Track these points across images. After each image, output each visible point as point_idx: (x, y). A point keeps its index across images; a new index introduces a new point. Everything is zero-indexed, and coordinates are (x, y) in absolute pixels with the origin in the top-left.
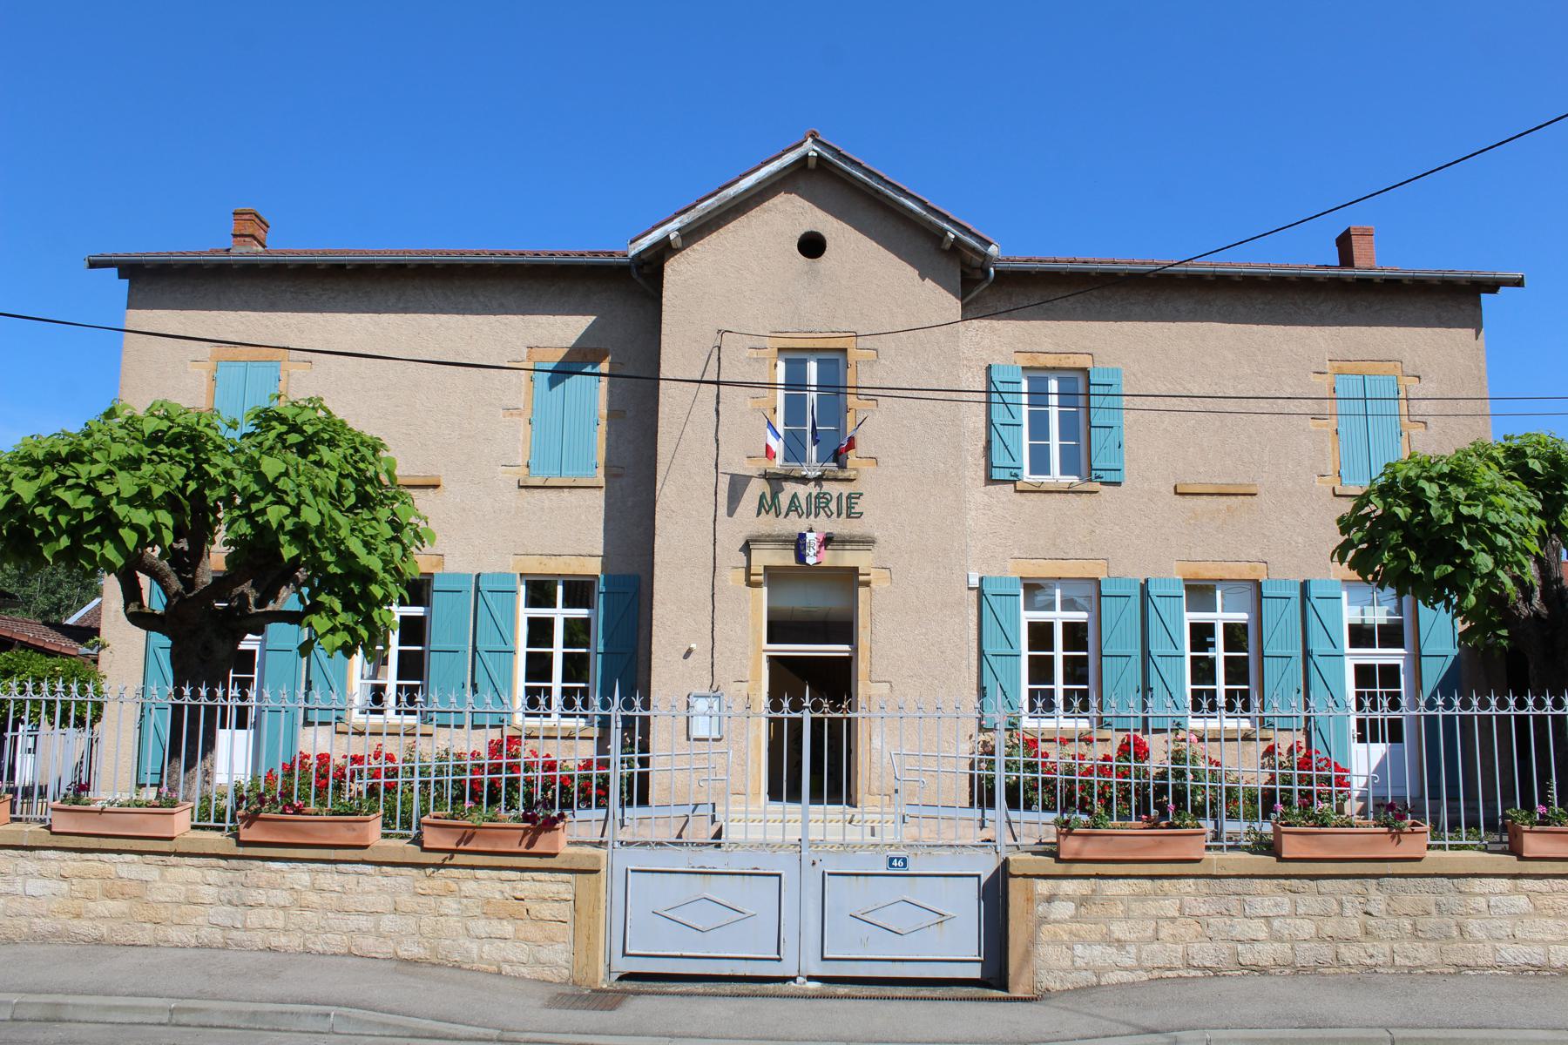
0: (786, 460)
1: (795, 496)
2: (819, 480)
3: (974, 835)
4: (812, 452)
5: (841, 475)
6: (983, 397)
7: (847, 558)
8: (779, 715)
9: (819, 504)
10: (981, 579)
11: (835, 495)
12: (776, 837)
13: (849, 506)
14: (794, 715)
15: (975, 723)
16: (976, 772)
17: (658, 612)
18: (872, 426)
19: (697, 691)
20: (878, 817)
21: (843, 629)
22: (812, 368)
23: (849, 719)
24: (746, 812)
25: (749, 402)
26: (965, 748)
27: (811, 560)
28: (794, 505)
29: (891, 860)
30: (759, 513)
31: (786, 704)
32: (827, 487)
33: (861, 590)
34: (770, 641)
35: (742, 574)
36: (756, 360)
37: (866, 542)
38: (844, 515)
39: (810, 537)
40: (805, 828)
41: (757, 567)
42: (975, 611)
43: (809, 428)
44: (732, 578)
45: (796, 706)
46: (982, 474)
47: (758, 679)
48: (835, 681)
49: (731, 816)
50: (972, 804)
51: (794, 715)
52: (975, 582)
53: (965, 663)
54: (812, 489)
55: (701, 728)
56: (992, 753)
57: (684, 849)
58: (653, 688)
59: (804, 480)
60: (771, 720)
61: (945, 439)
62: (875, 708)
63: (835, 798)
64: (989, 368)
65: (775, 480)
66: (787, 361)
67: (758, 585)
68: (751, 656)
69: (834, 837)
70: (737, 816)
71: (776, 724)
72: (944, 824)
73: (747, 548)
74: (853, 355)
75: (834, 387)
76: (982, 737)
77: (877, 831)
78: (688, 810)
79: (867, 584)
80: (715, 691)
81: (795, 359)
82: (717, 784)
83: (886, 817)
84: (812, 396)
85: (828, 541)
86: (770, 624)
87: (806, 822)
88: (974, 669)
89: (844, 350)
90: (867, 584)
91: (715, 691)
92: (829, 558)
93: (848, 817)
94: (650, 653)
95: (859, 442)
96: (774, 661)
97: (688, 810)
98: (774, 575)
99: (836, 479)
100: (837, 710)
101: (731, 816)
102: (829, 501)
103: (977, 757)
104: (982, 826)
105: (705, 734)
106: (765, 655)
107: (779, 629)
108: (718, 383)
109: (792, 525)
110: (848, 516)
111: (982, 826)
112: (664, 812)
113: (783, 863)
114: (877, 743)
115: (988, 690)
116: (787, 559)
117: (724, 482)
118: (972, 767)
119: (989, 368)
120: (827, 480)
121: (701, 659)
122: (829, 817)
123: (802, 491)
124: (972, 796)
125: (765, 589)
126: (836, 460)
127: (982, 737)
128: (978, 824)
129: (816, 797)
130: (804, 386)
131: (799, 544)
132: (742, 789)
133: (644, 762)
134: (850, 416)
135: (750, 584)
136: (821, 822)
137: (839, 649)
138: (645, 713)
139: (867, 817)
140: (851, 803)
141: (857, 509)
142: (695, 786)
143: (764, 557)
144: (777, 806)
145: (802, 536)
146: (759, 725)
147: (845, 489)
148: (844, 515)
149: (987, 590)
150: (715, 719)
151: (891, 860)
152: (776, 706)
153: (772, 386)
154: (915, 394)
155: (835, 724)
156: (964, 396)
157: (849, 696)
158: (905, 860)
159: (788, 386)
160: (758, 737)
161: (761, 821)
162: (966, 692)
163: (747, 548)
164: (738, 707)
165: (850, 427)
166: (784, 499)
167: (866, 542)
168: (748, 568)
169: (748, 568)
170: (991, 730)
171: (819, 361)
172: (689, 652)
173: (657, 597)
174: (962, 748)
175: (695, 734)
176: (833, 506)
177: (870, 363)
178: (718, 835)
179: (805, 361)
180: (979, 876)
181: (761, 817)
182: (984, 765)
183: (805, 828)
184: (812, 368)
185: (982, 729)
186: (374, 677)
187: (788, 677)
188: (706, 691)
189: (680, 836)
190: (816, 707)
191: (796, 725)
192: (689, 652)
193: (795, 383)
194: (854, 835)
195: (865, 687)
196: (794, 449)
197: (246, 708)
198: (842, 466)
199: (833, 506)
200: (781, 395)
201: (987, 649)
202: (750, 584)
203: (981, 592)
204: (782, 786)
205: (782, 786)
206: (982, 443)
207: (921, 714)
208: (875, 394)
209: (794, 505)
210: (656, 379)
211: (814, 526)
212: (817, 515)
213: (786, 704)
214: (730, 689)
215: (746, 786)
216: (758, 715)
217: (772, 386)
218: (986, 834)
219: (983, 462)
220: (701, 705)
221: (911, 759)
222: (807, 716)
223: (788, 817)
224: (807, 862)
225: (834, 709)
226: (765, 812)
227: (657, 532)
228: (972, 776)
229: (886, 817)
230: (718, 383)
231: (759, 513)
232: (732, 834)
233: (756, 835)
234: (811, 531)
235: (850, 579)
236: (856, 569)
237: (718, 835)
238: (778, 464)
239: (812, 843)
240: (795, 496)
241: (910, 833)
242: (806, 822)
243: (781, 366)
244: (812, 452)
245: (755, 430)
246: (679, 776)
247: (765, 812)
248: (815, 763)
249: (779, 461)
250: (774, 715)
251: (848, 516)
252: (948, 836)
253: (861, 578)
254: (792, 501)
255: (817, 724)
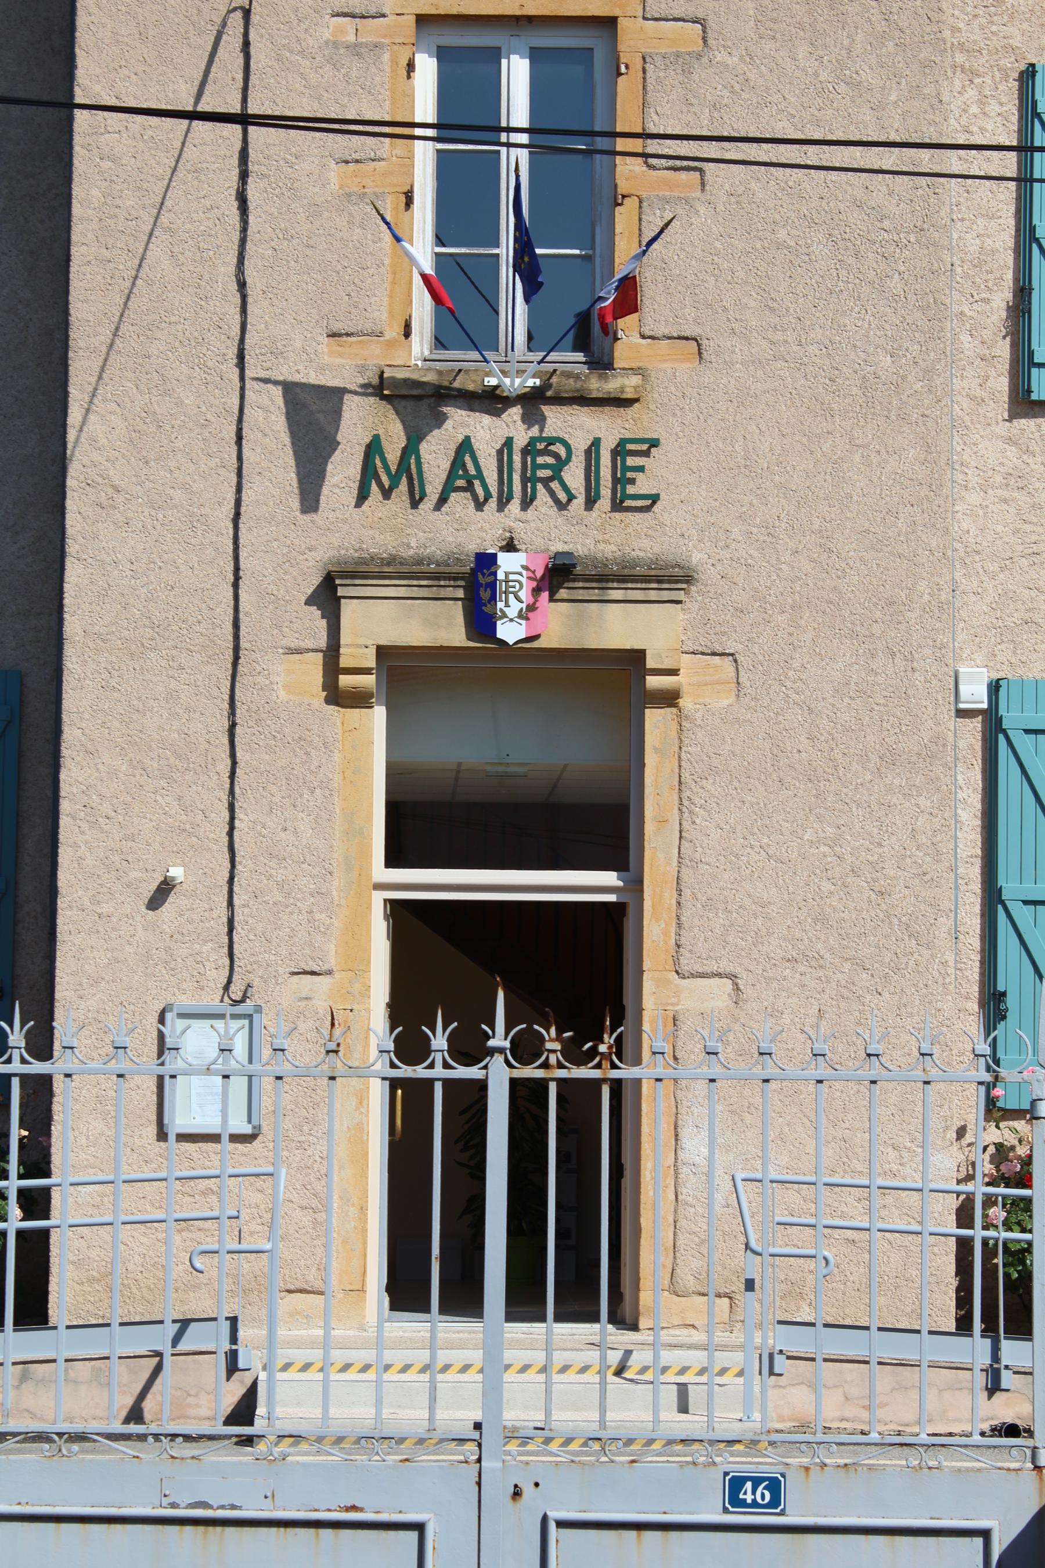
0: (439, 342)
1: (465, 447)
2: (533, 402)
3: (968, 1410)
4: (515, 314)
5: (596, 386)
6: (1008, 163)
7: (615, 625)
8: (420, 1072)
9: (535, 470)
10: (994, 688)
11: (580, 444)
12: (408, 1414)
13: (620, 481)
14: (463, 1072)
15: (976, 1098)
16: (978, 1234)
17: (75, 776)
18: (690, 247)
19: (185, 1001)
20: (697, 1358)
21: (602, 825)
22: (517, 74)
23: (617, 1086)
24: (326, 1344)
25: (334, 174)
26: (945, 1164)
27: (509, 632)
28: (462, 472)
29: (736, 1484)
30: (362, 497)
31: (439, 1042)
32: (558, 420)
33: (655, 719)
34: (394, 859)
35: (314, 668)
36: (355, 49)
37: (668, 579)
38: (604, 503)
39: (508, 563)
40: (492, 1394)
41: (359, 647)
42: (976, 776)
43: (506, 249)
44: (287, 680)
45: (469, 1048)
46: (1003, 384)
47: (359, 967)
48: (578, 975)
49: (283, 1355)
50: (964, 1325)
51: (463, 1072)
52: (975, 693)
53: (945, 923)
54: (512, 425)
55: (196, 1106)
56: (1024, 1180)
57: (148, 1452)
58: (61, 992)
59: (491, 401)
60: (394, 1084)
61: (895, 284)
62: (692, 1050)
63: (578, 1304)
64: (1028, 75)
65: (419, 401)
66: (443, 55)
67: (359, 700)
68: (337, 901)
69: (575, 1415)
70: (300, 1356)
71: (410, 1100)
72: (885, 1378)
73: (327, 596)
74: (633, 37)
75: (578, 138)
76: (993, 1135)
77: (695, 1395)
78: (160, 1338)
79: (669, 699)
80: (237, 1001)
81: (466, 52)
82: (247, 1265)
83: (723, 1359)
84: (516, 161)
85: (558, 575)
86: (394, 810)
87: (493, 1370)
88: (973, 941)
89: (609, 24)
90: (669, 699)
91: (237, 1001)
92: (560, 625)
93: (614, 1358)
94: (53, 892)
95: (649, 293)
96: (406, 917)
97: (160, 1338)
98: (403, 671)
99: (583, 400)
100: (581, 1059)
101: (283, 1355)
102: (561, 463)
103: (979, 1189)
104: (994, 1387)
105: (206, 1121)
106: (378, 898)
107: (414, 830)
108: (243, 120)
109: (460, 529)
110: (617, 506)
111: (994, 1387)
112: (93, 1344)
113: (432, 1494)
114: (695, 1146)
115: (1011, 1002)
116: (443, 626)
117: (269, 415)
118: (964, 1216)
119: (1028, 75)
120: (559, 400)
121: (197, 908)
122: (560, 1358)
123: (486, 432)
124: (964, 1300)
125: (379, 714)
126: (582, 343)
127: (993, 1135)
128: (981, 1380)
129: (523, 1302)
130: (492, 129)
131: (476, 585)
132: (318, 1285)
133: (36, 1203)
134: (624, 217)
135: (336, 696)
136: (537, 1371)
137: (592, 884)
138: (38, 1067)
139: (667, 1357)
140: (624, 1318)
141: (643, 485)
142: (179, 1270)
143: (375, 622)
144: (411, 1327)
145: (486, 562)
146: (362, 1099)
147: (606, 427)
148: (604, 503)
149: (1011, 717)
150: (239, 1084)
151: (736, 1484)
152: (410, 1047)
153: (402, 129)
154: (813, 155)
155: (579, 1098)
156: (954, 162)
157: (618, 1020)
158: (774, 1486)
159: (446, 128)
160: (359, 1131)
161: (366, 1372)
162: (947, 1006)
163: (327, 596)
164: (305, 1051)
165: (625, 249)
166: (436, 455)
167: (668, 579)
168: (332, 651)
169: (332, 651)
170: (1017, 1114)
171: (536, 56)
172: (165, 889)
173: (70, 734)
174: (936, 1161)
175: (180, 1121)
176: (574, 476)
177: (683, 62)
178: (244, 1412)
179: (494, 56)
180: (985, 1534)
181: (368, 1355)
182: (998, 1213)
183: (492, 1394)
184: (517, 74)
185: (995, 1111)
186: (996, 1227)
187: (445, 963)
188: (211, 1000)
189: (135, 1415)
190: (525, 1049)
191: (469, 1100)
192: (165, 889)
193: (467, 119)
194: (632, 1409)
195: (661, 993)
196: (461, 303)
197: (46, 1081)
198: (602, 364)
199: (574, 476)
200: (424, 156)
201: (1010, 886)
202: (336, 696)
203: (993, 724)
204: (428, 1270)
205: (428, 1270)
206: (1003, 296)
207: (822, 1071)
208: (691, 156)
209: (462, 472)
210: (66, 106)
211: (521, 533)
212: (527, 503)
213: (439, 1042)
214: (281, 997)
215: (324, 1269)
216: (362, 1073)
217: (402, 129)
218: (1005, 1409)
219: (1003, 349)
220: (198, 1041)
221: (792, 1196)
222: (498, 1077)
223: (443, 1357)
224: (496, 1490)
225: (574, 1055)
226: (379, 1344)
227: (72, 547)
228: (964, 1246)
229: (723, 1359)
230: (243, 120)
231: (362, 497)
232: (285, 1406)
233: (353, 1408)
234: (510, 547)
235: (621, 682)
236: (638, 656)
237: (244, 1412)
238: (417, 355)
239: (511, 1435)
240: (465, 447)
241: (791, 1399)
242: (493, 1370)
243: (427, 66)
244: (515, 314)
245: (358, 266)
246: (138, 1243)
247: (379, 1344)
248: (518, 1191)
249: (420, 345)
250: (406, 1071)
251: (617, 506)
252: (898, 1409)
253: (653, 682)
254: (457, 463)
255: (526, 1098)
